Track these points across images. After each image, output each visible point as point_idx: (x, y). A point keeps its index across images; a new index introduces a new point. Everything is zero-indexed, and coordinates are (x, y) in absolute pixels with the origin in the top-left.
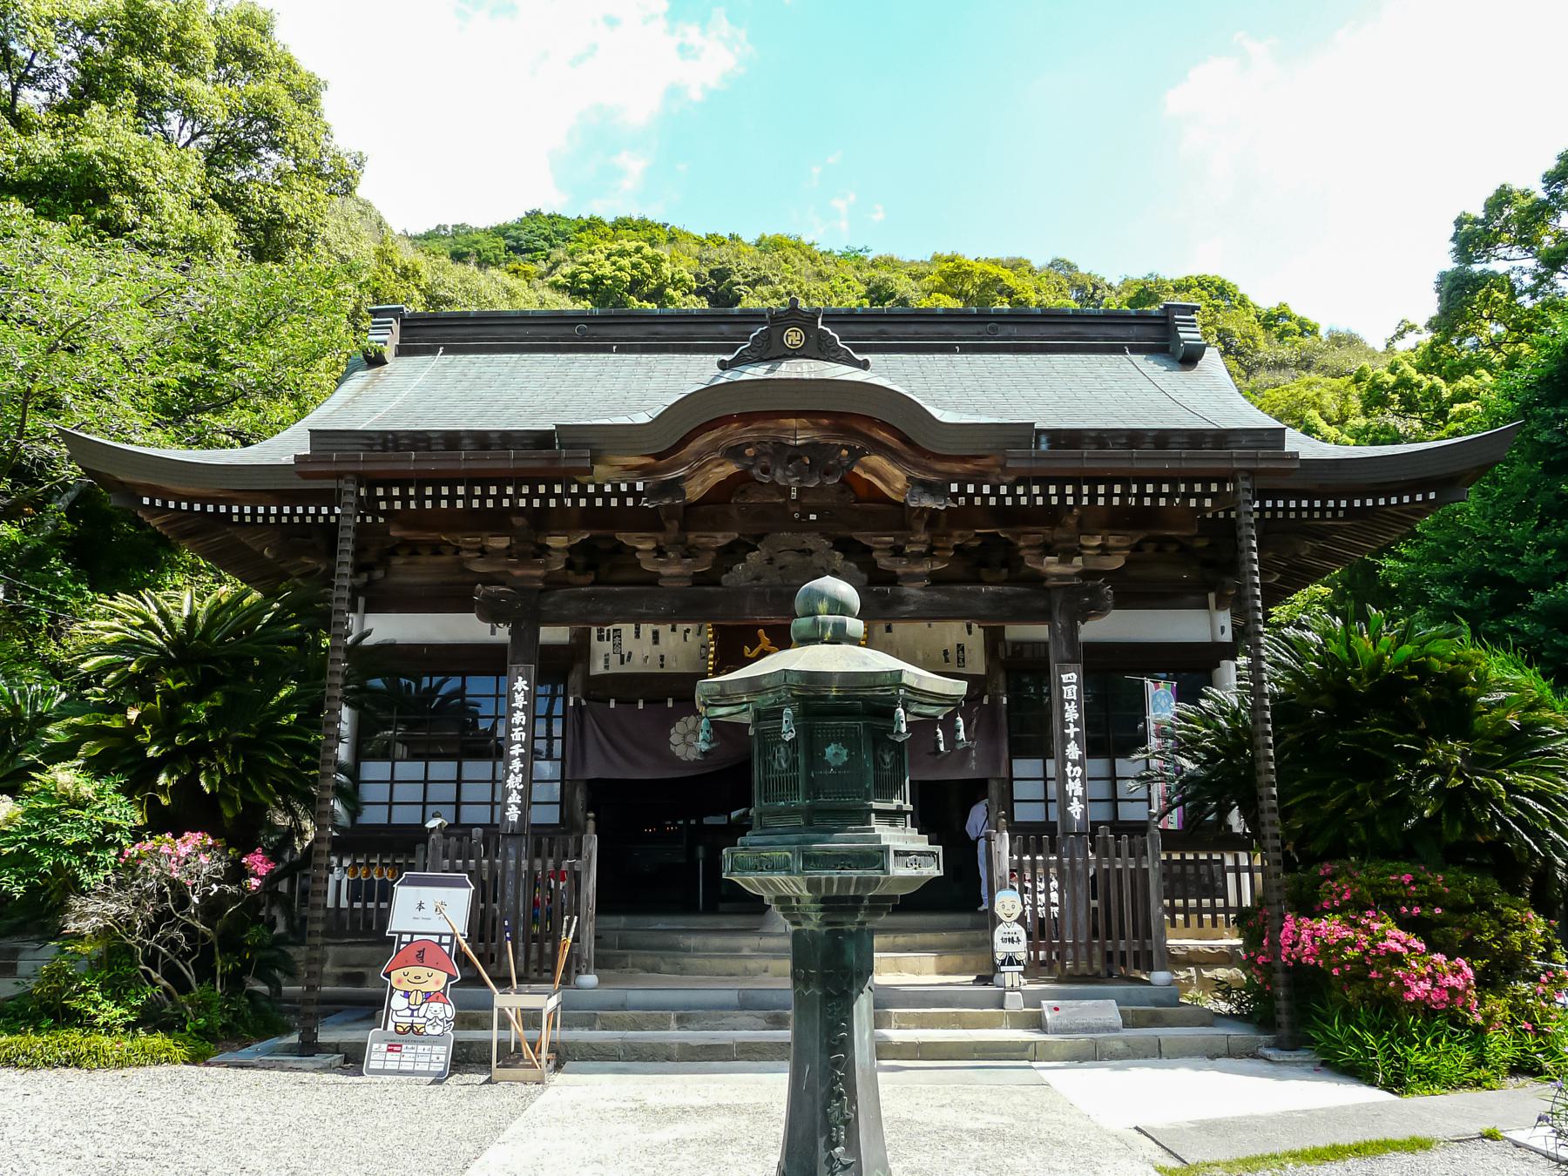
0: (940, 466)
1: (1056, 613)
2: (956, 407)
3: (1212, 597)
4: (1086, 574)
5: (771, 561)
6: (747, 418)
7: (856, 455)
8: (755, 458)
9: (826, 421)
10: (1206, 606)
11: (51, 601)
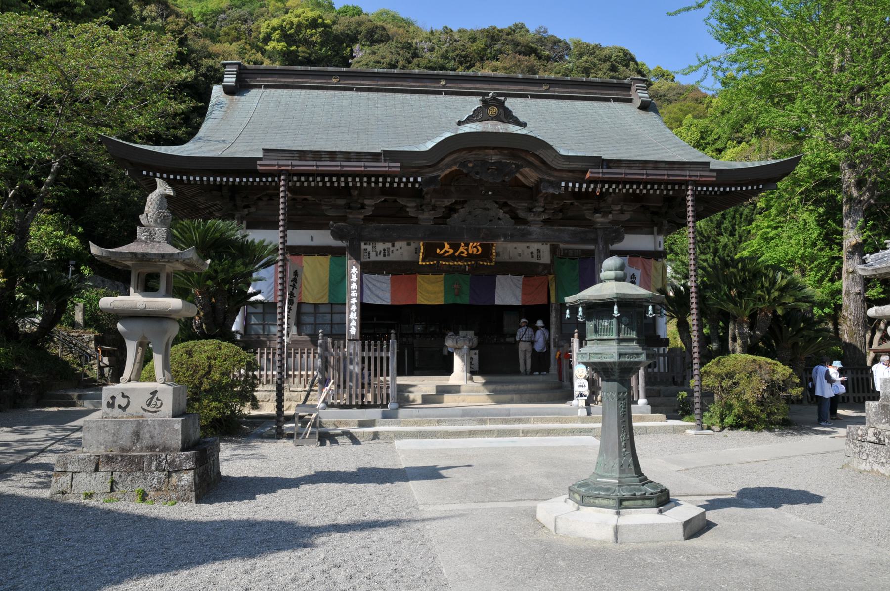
0: (556, 174)
1: (600, 240)
2: (568, 150)
3: (655, 229)
4: (613, 222)
5: (470, 213)
6: (470, 149)
7: (518, 167)
8: (472, 167)
9: (506, 152)
10: (652, 233)
11: (718, 298)
